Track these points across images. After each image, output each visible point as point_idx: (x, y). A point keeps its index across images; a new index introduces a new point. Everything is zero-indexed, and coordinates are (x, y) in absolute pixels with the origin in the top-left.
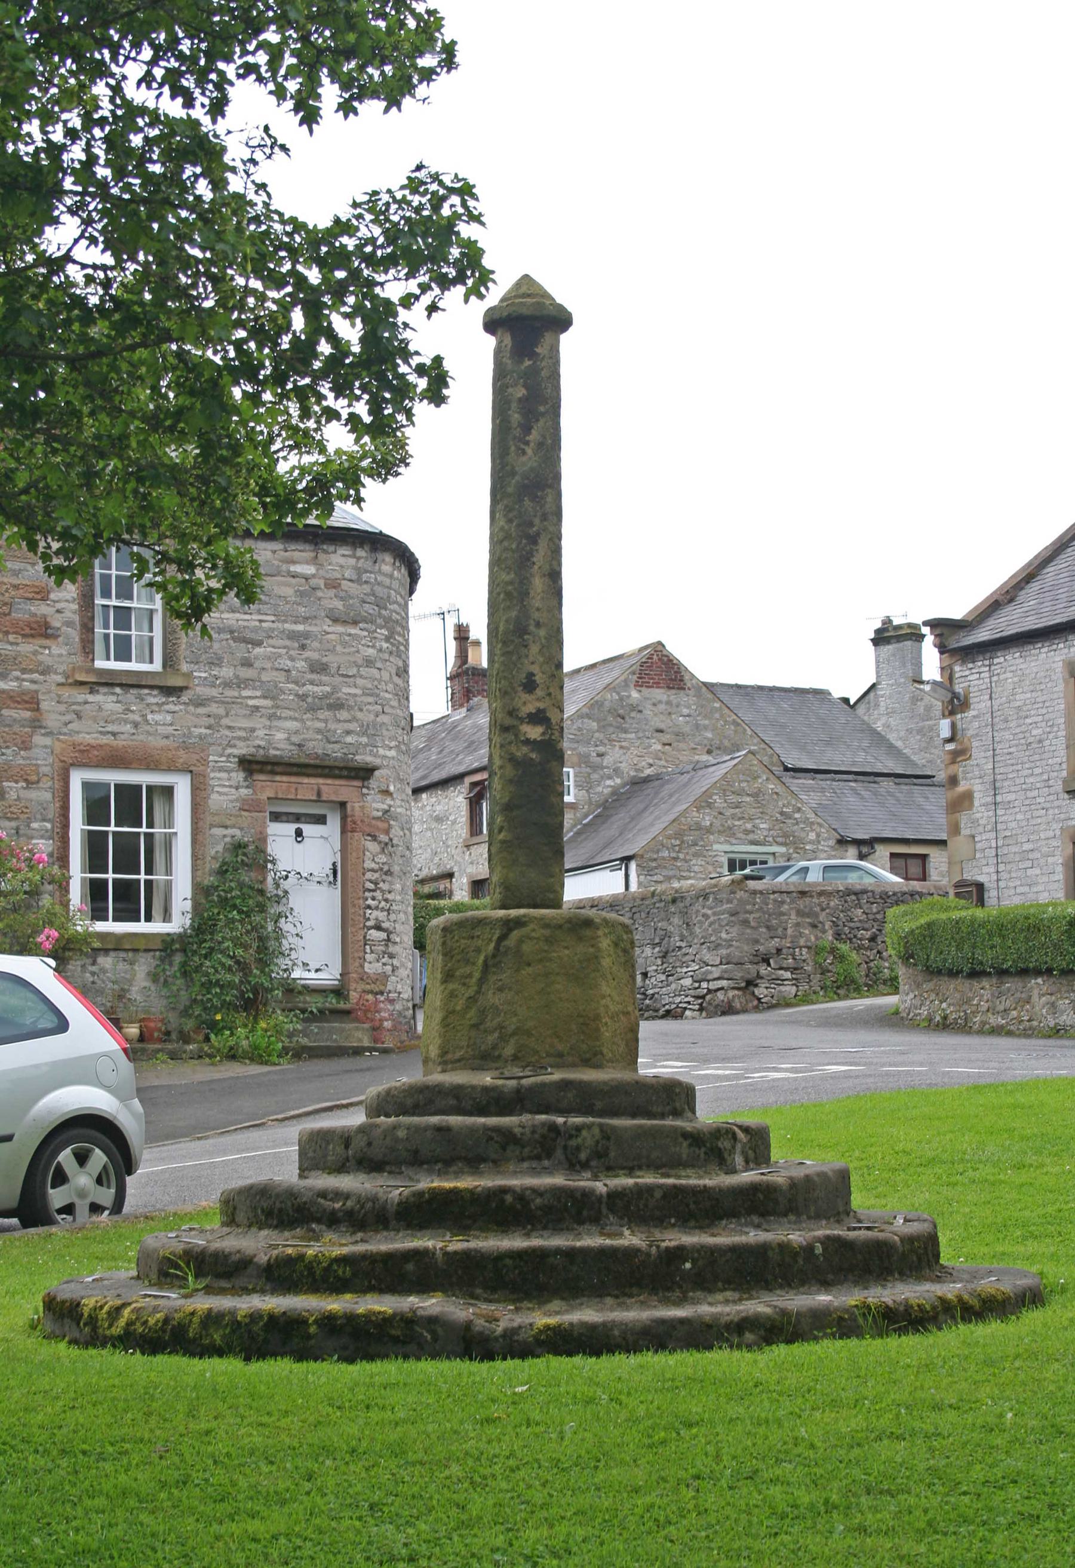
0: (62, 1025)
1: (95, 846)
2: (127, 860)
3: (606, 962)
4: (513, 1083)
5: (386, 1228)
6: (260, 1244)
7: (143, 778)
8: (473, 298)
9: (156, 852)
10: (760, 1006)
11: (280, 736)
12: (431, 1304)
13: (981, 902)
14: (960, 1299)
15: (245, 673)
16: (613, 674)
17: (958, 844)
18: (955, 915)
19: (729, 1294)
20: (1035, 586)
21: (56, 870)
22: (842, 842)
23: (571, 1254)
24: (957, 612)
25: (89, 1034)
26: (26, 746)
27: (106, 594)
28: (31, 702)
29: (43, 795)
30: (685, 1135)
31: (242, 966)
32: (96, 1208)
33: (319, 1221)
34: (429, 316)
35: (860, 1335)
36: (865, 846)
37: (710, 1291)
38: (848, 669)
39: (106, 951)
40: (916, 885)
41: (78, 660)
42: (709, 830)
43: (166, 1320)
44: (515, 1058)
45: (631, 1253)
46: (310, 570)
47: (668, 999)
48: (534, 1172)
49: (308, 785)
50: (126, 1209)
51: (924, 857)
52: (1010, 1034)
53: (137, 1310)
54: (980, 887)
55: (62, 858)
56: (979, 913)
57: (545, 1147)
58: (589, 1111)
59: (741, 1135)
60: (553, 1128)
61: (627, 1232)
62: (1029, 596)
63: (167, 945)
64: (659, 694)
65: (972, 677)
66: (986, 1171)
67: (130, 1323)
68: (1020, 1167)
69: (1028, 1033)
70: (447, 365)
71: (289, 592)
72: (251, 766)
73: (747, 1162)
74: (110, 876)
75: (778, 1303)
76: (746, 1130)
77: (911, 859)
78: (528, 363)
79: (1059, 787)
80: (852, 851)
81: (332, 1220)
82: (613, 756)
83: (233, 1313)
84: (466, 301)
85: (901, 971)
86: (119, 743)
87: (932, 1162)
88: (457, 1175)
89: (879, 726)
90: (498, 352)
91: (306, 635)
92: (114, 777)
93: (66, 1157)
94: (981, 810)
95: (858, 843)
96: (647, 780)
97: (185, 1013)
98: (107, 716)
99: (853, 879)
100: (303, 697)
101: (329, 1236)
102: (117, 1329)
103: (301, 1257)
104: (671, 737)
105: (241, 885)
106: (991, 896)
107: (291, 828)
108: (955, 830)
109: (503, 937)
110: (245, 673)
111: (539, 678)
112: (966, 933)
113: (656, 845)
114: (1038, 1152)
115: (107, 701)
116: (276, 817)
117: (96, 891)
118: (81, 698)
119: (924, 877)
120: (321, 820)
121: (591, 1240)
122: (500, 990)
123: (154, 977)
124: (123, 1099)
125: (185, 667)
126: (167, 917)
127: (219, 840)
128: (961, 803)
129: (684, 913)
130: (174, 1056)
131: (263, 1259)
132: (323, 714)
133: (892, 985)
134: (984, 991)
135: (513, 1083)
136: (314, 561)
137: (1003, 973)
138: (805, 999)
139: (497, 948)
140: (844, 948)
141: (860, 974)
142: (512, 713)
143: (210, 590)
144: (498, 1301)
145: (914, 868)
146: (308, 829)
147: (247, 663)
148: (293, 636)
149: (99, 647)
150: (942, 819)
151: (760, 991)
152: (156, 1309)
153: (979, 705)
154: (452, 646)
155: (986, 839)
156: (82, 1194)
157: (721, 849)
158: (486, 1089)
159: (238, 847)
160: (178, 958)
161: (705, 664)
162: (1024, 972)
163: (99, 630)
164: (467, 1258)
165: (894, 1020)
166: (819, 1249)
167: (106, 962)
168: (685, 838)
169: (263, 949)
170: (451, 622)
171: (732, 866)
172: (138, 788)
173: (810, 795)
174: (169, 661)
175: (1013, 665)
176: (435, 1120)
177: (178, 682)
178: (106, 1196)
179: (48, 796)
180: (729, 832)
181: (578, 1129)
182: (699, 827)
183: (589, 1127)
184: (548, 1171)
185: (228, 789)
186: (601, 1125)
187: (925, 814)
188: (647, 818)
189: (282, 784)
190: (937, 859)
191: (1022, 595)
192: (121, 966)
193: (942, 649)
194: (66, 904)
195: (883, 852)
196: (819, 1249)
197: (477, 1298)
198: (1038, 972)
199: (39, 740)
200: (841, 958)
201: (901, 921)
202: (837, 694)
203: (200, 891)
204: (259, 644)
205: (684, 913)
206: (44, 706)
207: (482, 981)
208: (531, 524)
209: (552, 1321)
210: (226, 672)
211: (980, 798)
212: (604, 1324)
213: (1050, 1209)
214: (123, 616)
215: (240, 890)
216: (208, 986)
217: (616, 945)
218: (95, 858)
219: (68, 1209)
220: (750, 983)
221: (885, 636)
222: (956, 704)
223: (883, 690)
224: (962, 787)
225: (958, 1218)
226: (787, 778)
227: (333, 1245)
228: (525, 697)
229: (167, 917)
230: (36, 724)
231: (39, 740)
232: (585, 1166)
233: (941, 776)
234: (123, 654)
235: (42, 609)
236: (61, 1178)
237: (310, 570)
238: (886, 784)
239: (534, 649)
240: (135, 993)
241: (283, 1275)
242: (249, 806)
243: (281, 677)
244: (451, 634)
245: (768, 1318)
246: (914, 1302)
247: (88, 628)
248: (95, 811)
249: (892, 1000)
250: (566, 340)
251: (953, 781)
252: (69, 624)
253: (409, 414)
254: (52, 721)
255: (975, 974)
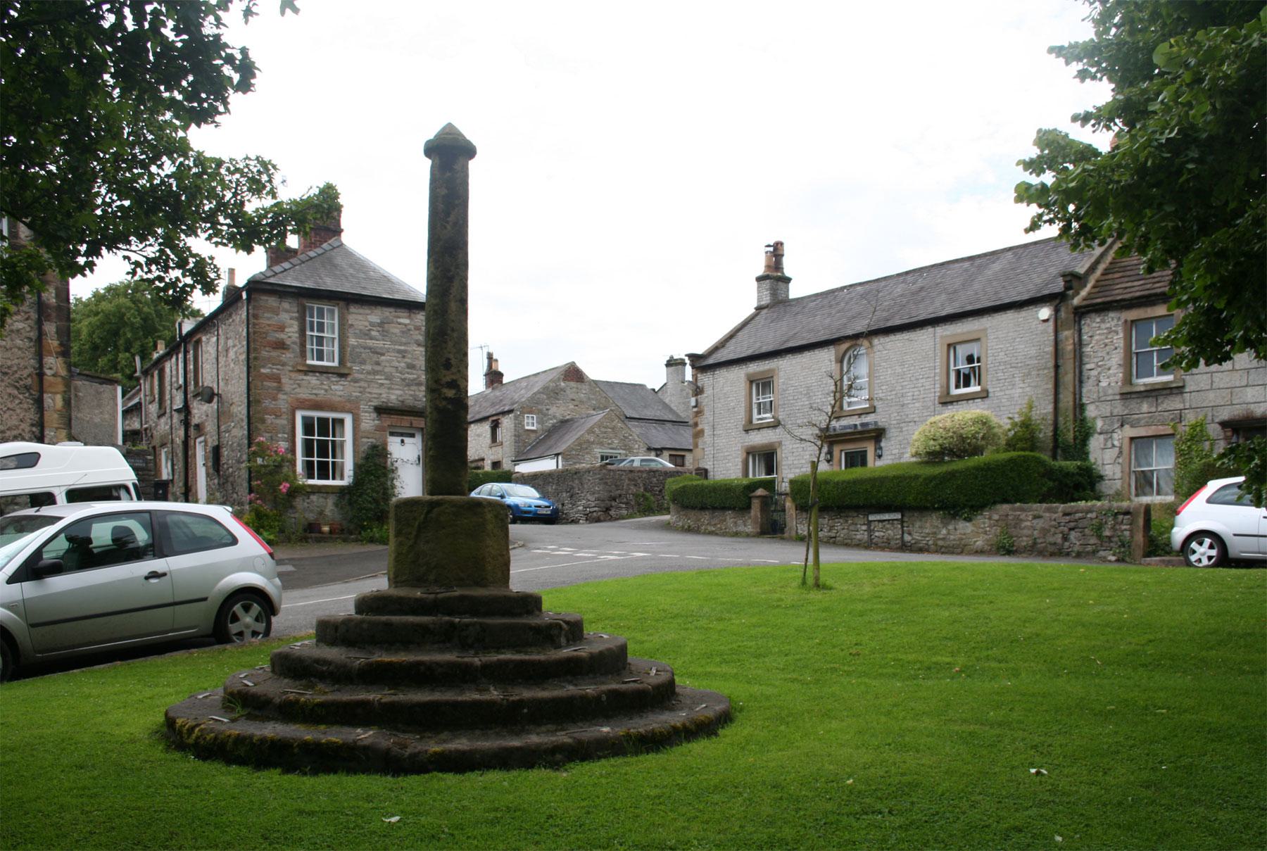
0: (234, 541)
1: (308, 446)
2: (323, 452)
3: (490, 527)
4: (432, 596)
5: (352, 683)
6: (334, 654)
7: (331, 415)
8: (288, 11)
9: (337, 448)
10: (612, 519)
11: (393, 397)
12: (364, 735)
13: (706, 477)
14: (684, 725)
15: (377, 368)
16: (554, 375)
17: (698, 452)
18: (695, 483)
19: (551, 727)
20: (733, 340)
21: (289, 456)
22: (649, 449)
23: (455, 705)
24: (700, 351)
25: (249, 544)
26: (275, 399)
27: (312, 330)
28: (277, 379)
29: (283, 422)
30: (531, 628)
31: (376, 501)
32: (255, 634)
33: (315, 676)
34: (246, 22)
35: (624, 754)
36: (659, 451)
37: (539, 725)
38: (655, 378)
39: (314, 493)
40: (679, 468)
41: (299, 360)
42: (593, 443)
43: (216, 738)
44: (436, 581)
45: (491, 704)
46: (407, 321)
47: (573, 515)
48: (442, 651)
49: (406, 420)
50: (272, 634)
51: (683, 457)
52: (717, 534)
53: (201, 730)
54: (706, 471)
55: (293, 451)
56: (706, 482)
57: (448, 637)
58: (474, 614)
59: (565, 626)
60: (452, 625)
61: (492, 688)
62: (731, 346)
63: (342, 491)
64: (573, 384)
65: (706, 380)
66: (703, 622)
67: (198, 738)
68: (720, 619)
69: (724, 534)
70: (253, 55)
71: (396, 331)
72: (381, 410)
73: (568, 641)
74: (316, 459)
75: (576, 735)
76: (567, 623)
77: (678, 457)
78: (448, 174)
79: (741, 428)
80: (653, 453)
81: (322, 677)
82: (553, 410)
83: (251, 737)
84: (283, 13)
85: (672, 506)
86: (318, 399)
87: (676, 616)
88: (397, 651)
89: (667, 401)
90: (432, 167)
91: (405, 351)
92: (316, 414)
93: (237, 608)
94: (707, 438)
95: (656, 450)
96: (567, 421)
97: (350, 521)
98: (312, 387)
99: (653, 465)
100: (404, 380)
101: (320, 686)
102: (191, 741)
103: (297, 701)
104: (578, 403)
105: (375, 465)
106: (711, 474)
107: (398, 439)
108: (696, 446)
109: (428, 512)
110: (377, 368)
111: (453, 361)
112: (699, 491)
113: (570, 449)
114: (729, 612)
115: (313, 380)
116: (392, 434)
117: (309, 466)
118: (301, 377)
119: (683, 465)
120: (412, 436)
121: (472, 696)
122: (427, 542)
123: (336, 505)
124: (269, 578)
125: (349, 365)
126: (342, 478)
127: (366, 442)
128: (699, 434)
129: (580, 479)
130: (345, 540)
131: (277, 700)
132: (413, 388)
133: (668, 511)
134: (705, 517)
135: (432, 596)
136: (409, 317)
137: (714, 508)
138: (631, 516)
139: (425, 518)
140: (648, 494)
141: (654, 506)
142: (437, 381)
143: (186, 285)
144: (410, 732)
145: (679, 460)
146: (407, 440)
147: (378, 364)
148: (399, 351)
149: (309, 354)
150: (691, 441)
151: (612, 513)
152: (212, 731)
153: (708, 392)
154: (486, 361)
155: (709, 450)
156: (247, 626)
157: (598, 451)
158: (417, 600)
159: (374, 447)
160: (347, 497)
161: (593, 372)
162: (724, 509)
163: (308, 347)
164: (392, 706)
165: (667, 527)
166: (604, 698)
167: (314, 498)
168: (583, 446)
169: (384, 494)
170: (485, 351)
171: (602, 458)
172: (327, 419)
173: (636, 429)
174: (341, 361)
175: (724, 375)
176: (384, 618)
177: (346, 371)
178: (261, 627)
179: (285, 422)
180: (601, 444)
181: (467, 625)
182: (588, 441)
183: (474, 624)
184: (449, 650)
185: (369, 421)
186: (481, 624)
187: (683, 438)
188: (567, 437)
189: (394, 419)
190: (689, 458)
191: (728, 345)
192: (321, 500)
193: (693, 367)
194: (294, 472)
195: (666, 454)
196: (604, 698)
197: (398, 730)
198: (729, 509)
199: (281, 396)
200: (646, 499)
201: (672, 485)
202: (650, 387)
203: (358, 468)
204: (383, 354)
205: (580, 479)
206: (283, 381)
207: (417, 536)
208: (449, 271)
209: (437, 748)
210: (368, 367)
211: (707, 432)
212: (470, 751)
213: (734, 646)
214: (320, 340)
215: (374, 466)
216: (360, 509)
217: (496, 517)
218: (308, 450)
219: (240, 634)
220: (608, 509)
221: (671, 363)
222: (698, 391)
223: (669, 386)
224: (700, 427)
225: (688, 649)
226: (626, 421)
227: (272, 730)
228: (444, 372)
229: (342, 478)
230: (279, 389)
231: (281, 396)
232: (471, 647)
233: (691, 422)
234: (320, 358)
235: (282, 336)
236: (235, 619)
237: (407, 321)
238: (669, 425)
239: (450, 344)
240: (327, 512)
241: (289, 711)
242: (379, 429)
243: (393, 370)
244: (485, 356)
245: (570, 745)
246: (657, 731)
247: (303, 345)
248: (308, 429)
249: (667, 517)
250: (472, 164)
251: (696, 424)
252: (294, 343)
253: (225, 103)
254: (287, 388)
255: (703, 508)
